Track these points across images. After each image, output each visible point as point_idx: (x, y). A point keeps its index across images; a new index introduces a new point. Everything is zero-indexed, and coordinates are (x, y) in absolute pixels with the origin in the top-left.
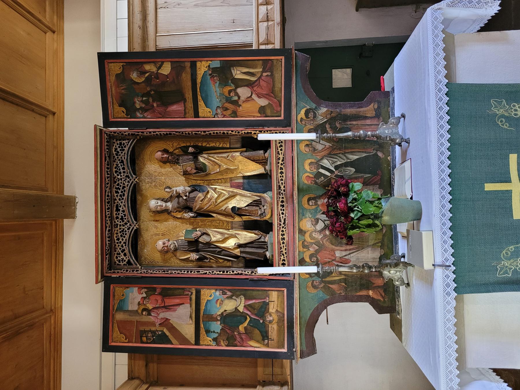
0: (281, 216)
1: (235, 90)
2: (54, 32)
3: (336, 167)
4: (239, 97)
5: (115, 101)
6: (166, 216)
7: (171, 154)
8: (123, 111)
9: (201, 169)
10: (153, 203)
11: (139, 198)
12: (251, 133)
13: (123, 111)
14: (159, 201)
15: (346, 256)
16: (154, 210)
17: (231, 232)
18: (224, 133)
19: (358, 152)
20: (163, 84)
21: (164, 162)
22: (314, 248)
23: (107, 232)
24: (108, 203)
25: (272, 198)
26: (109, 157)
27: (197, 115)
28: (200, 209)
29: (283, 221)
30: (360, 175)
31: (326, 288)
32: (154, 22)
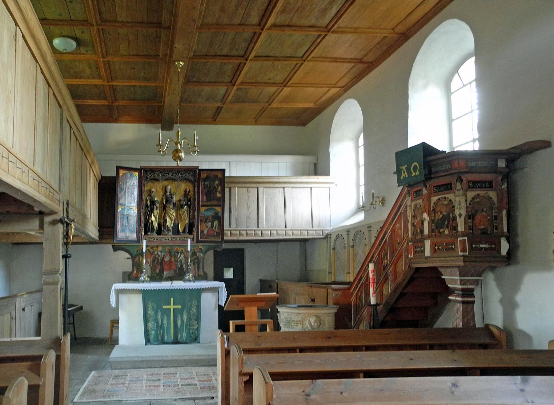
3: (181, 260)
6: (164, 191)
7: (188, 194)
9: (182, 207)
10: (169, 187)
21: (185, 191)
27: (202, 206)
31: (136, 255)
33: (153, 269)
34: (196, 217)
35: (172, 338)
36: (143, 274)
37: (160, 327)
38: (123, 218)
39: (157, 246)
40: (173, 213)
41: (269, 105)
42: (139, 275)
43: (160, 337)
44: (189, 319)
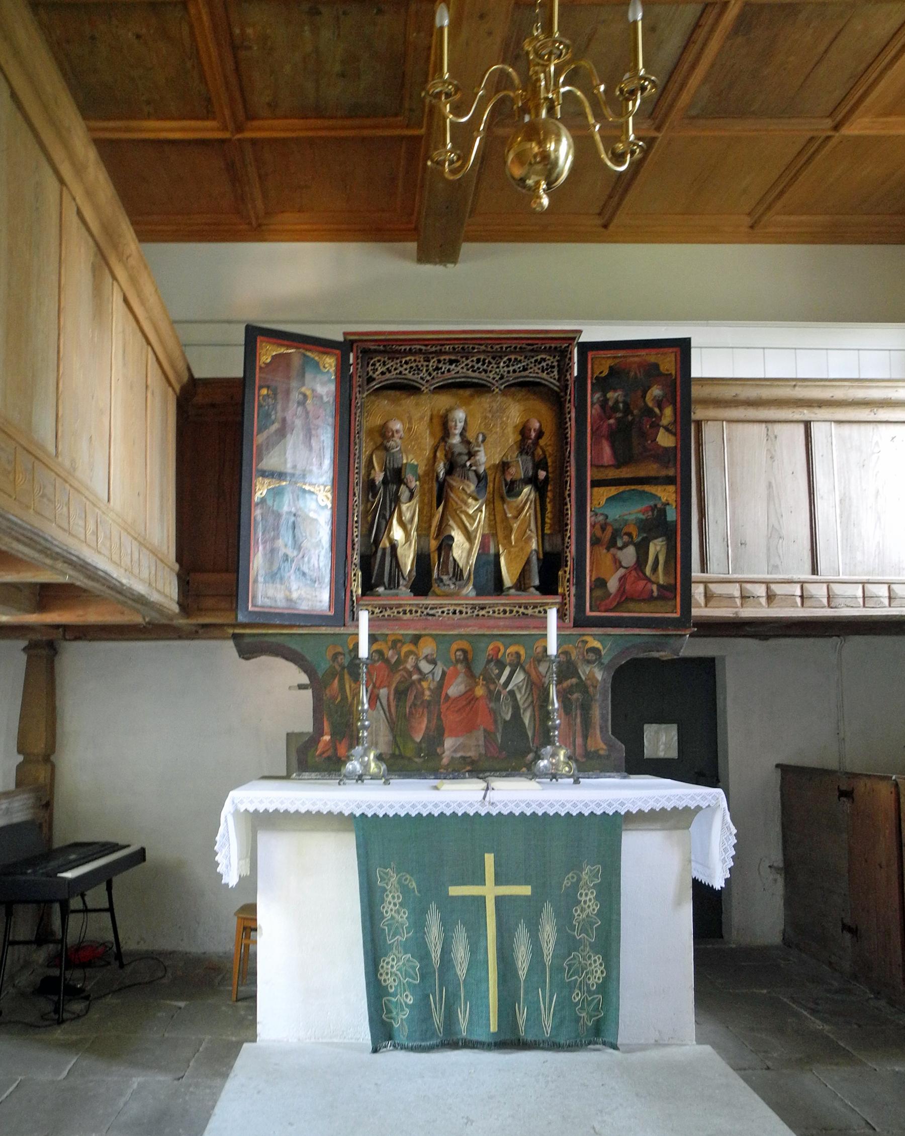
0: (440, 611)
1: (631, 542)
2: (752, 227)
3: (512, 693)
4: (621, 549)
5: (617, 361)
6: (439, 435)
8: (601, 373)
9: (512, 489)
11: (468, 392)
12: (566, 566)
13: (601, 373)
14: (462, 424)
15: (381, 703)
16: (450, 416)
17: (414, 534)
18: (567, 525)
19: (535, 727)
20: (643, 435)
21: (524, 431)
22: (392, 657)
23: (418, 347)
24: (463, 348)
25: (466, 597)
26: (532, 350)
27: (596, 484)
28: (451, 488)
29: (432, 612)
30: (500, 727)
31: (332, 674)
32: (745, 418)
33: (399, 727)
34: (572, 526)
35: (494, 1028)
36: (359, 749)
37: (435, 976)
38: (276, 528)
39: (416, 639)
40: (476, 512)
41: (836, 128)
42: (342, 751)
43: (438, 1019)
44: (568, 944)
